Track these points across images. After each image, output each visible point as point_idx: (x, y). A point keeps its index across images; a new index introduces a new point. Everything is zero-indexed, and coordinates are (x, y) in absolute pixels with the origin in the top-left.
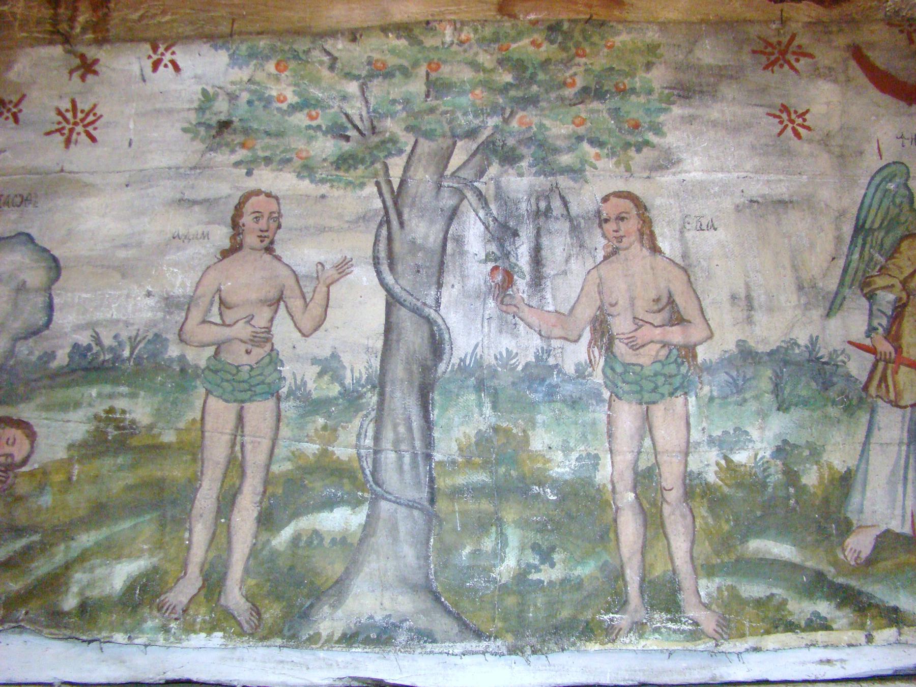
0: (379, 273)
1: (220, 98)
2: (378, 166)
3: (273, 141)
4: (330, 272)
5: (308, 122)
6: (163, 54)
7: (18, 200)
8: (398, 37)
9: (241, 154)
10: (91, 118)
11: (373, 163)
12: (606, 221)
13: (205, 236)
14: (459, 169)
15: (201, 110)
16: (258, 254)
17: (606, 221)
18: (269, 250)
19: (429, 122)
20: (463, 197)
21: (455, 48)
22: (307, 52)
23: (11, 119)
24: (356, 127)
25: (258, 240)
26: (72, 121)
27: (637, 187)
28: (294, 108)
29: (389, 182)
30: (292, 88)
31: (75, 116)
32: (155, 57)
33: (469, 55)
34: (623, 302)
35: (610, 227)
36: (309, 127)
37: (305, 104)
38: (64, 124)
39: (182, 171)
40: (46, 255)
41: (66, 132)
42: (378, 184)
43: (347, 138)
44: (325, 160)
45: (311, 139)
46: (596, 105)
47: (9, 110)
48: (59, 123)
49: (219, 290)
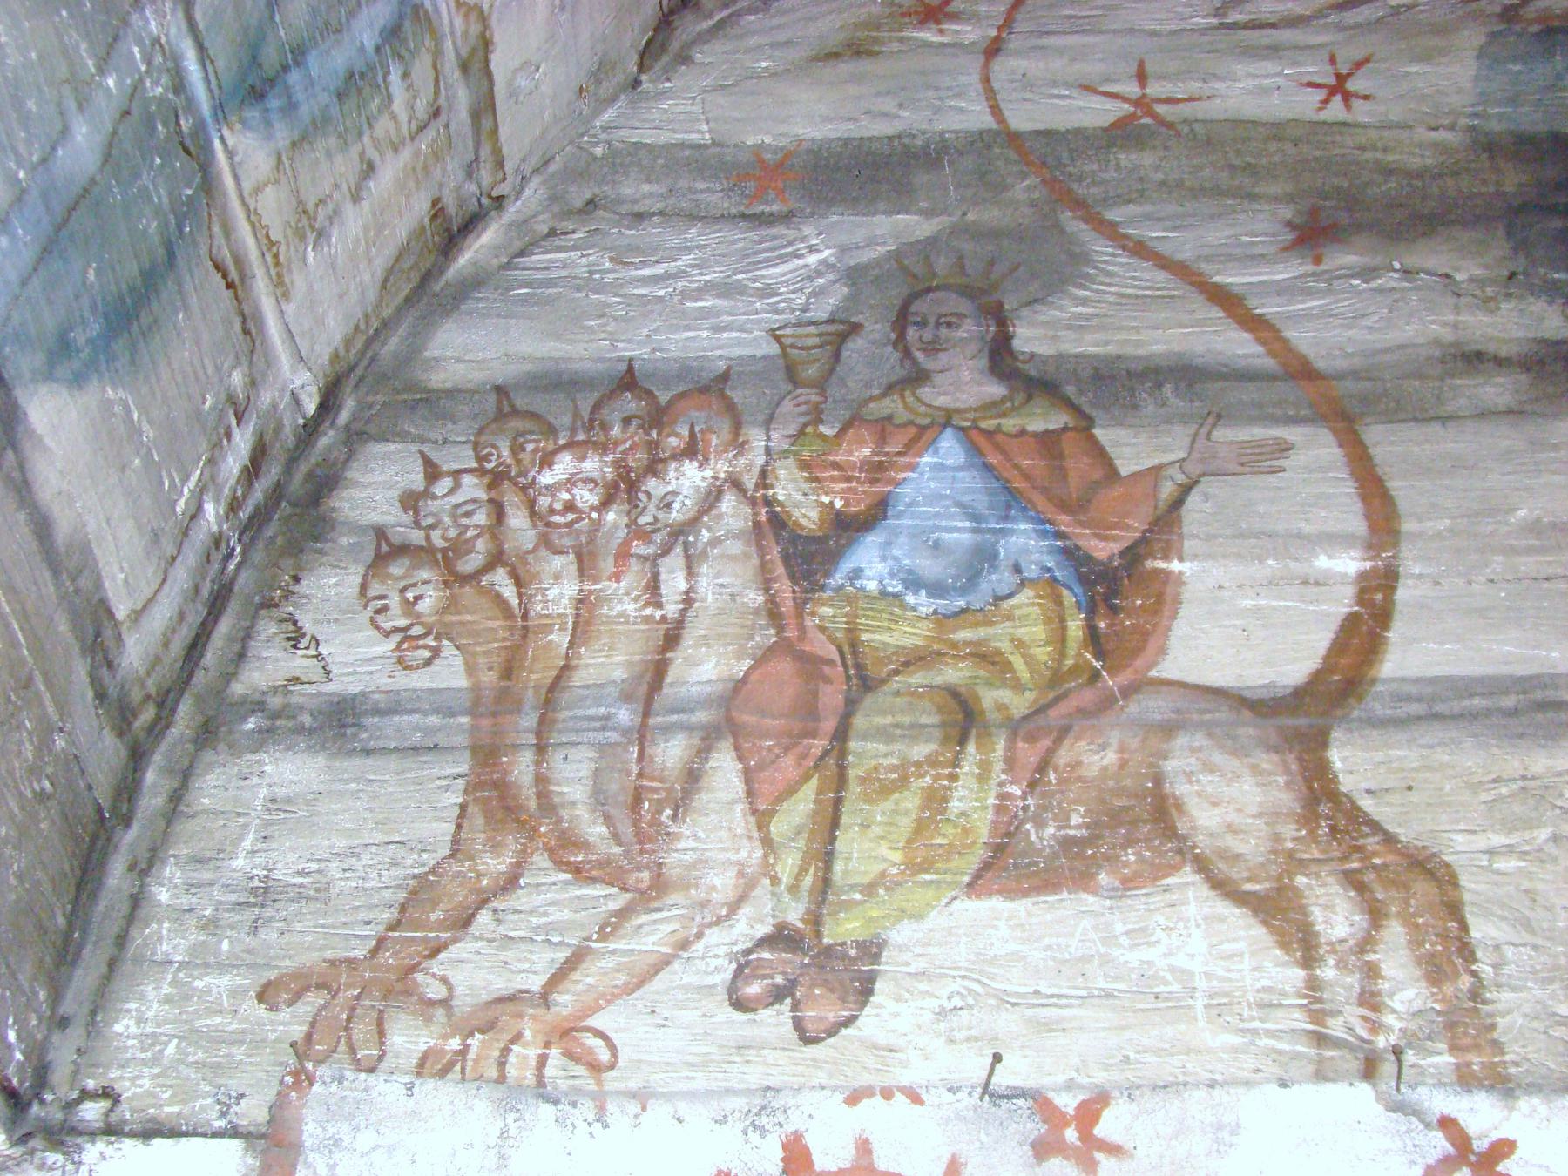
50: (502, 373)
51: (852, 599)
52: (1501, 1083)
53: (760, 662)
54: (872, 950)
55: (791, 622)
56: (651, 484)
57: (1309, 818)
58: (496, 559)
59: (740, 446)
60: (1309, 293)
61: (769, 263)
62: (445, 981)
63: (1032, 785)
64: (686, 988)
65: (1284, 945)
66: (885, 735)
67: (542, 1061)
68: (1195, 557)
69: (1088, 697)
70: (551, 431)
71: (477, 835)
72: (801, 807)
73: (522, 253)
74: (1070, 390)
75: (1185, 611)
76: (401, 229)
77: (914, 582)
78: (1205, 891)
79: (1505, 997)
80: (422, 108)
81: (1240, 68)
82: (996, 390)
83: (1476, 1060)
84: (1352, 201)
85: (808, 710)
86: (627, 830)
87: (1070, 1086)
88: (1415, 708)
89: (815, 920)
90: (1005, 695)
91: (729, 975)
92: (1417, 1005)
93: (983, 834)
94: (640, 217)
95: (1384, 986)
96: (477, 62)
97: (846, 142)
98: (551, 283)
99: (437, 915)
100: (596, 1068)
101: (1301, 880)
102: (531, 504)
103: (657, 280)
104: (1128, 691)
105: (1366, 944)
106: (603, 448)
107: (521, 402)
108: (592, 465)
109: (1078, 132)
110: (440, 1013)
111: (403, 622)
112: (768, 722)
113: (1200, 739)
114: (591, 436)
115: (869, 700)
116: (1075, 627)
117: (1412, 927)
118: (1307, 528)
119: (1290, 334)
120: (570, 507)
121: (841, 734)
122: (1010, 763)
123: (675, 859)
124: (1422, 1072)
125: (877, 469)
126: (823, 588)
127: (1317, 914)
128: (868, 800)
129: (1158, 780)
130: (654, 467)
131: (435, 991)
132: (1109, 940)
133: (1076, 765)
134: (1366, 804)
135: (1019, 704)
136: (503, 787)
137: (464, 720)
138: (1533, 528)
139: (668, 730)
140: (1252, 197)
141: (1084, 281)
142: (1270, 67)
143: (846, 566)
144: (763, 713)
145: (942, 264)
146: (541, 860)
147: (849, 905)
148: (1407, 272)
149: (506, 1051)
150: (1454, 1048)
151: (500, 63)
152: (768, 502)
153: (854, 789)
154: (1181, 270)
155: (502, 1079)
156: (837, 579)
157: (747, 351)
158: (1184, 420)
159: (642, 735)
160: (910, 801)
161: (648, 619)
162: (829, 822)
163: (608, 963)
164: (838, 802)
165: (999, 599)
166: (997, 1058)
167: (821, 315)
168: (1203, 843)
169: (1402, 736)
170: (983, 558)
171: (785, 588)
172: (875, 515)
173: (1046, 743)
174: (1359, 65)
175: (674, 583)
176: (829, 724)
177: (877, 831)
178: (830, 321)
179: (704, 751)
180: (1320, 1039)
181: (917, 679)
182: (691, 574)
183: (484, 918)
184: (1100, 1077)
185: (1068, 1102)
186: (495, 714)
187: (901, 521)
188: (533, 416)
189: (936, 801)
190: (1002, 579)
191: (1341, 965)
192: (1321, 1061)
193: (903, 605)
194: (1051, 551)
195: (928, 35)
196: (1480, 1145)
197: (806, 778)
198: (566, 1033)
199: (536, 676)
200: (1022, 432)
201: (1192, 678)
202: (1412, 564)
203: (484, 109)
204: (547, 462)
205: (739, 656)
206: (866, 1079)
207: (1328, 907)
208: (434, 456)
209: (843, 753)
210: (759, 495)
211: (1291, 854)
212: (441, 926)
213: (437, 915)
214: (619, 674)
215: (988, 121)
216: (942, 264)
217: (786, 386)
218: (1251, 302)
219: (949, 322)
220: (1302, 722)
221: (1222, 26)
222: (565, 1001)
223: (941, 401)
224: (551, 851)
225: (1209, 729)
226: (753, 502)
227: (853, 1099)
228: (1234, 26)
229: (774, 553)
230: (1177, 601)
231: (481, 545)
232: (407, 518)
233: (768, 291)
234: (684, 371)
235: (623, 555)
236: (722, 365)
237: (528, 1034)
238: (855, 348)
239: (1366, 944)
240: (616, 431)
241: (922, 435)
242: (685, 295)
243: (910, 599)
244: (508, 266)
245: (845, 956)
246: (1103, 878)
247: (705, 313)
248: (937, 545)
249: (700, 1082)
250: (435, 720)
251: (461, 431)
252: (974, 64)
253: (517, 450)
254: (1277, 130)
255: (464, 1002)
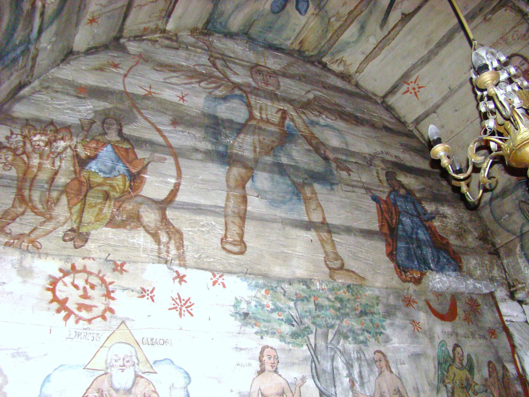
0: (315, 382)
1: (243, 302)
2: (306, 338)
3: (267, 324)
4: (300, 382)
5: (278, 317)
6: (218, 279)
7: (162, 342)
8: (303, 285)
9: (256, 329)
10: (188, 304)
11: (304, 336)
12: (376, 361)
13: (250, 365)
14: (331, 340)
15: (235, 306)
16: (272, 373)
17: (376, 361)
18: (276, 371)
19: (318, 321)
20: (336, 352)
21: (321, 291)
22: (276, 287)
23: (150, 299)
24: (295, 321)
25: (271, 367)
26: (180, 304)
27: (382, 349)
28: (273, 311)
29: (311, 344)
30: (271, 302)
31: (181, 302)
32: (214, 279)
33: (326, 295)
34: (386, 391)
35: (378, 363)
36: (279, 319)
37: (277, 309)
38: (176, 305)
39: (234, 334)
40: (182, 370)
41: (178, 309)
42: (307, 345)
43: (293, 325)
44: (287, 334)
45: (280, 325)
46: (365, 318)
47: (148, 295)
48: (174, 304)
49: (260, 389)
50: (27, 116)
51: (90, 172)
52: (185, 266)
53: (72, 180)
54: (88, 234)
55: (78, 174)
56: (55, 144)
57: (162, 221)
58: (24, 153)
59: (72, 140)
60: (174, 133)
61: (80, 106)
62: (10, 230)
63: (118, 210)
64: (55, 237)
65: (155, 242)
66: (93, 197)
67: (28, 246)
68: (149, 175)
69: (128, 196)
70: (36, 130)
71: (17, 204)
72: (77, 208)
73: (33, 93)
74: (131, 141)
75: (146, 184)
76: (13, 86)
77: (101, 171)
78: (144, 231)
79: (188, 253)
80: (23, 64)
81: (167, 90)
82: (118, 139)
83: (182, 263)
84: (181, 118)
85: (79, 191)
86: (46, 207)
87: (119, 260)
88: (180, 206)
89: (78, 228)
90: (114, 193)
91: (63, 235)
92: (174, 253)
93: (109, 217)
94: (57, 92)
95: (170, 250)
96: (34, 59)
97: (97, 86)
98: (38, 101)
99: (9, 218)
100: (38, 248)
101: (159, 232)
102: (31, 143)
103: (60, 105)
104: (135, 196)
105: (168, 243)
106: (46, 135)
107: (31, 123)
108: (43, 138)
109: (138, 95)
110: (9, 236)
111: (5, 161)
112: (73, 192)
113: (146, 206)
114: (43, 133)
115: (91, 191)
116: (128, 184)
117: (175, 240)
118: (167, 173)
119: (169, 139)
120: (39, 145)
121: (85, 196)
122: (114, 205)
123: (54, 213)
124: (174, 264)
125: (96, 149)
126: (84, 169)
127: (161, 237)
128: (89, 208)
129: (139, 212)
130: (55, 141)
131: (8, 231)
132: (128, 237)
133: (125, 207)
134: (171, 221)
135: (117, 195)
136: (23, 196)
137: (16, 182)
138: (202, 180)
139: (55, 190)
140: (166, 114)
141: (136, 122)
142: (171, 91)
143: (90, 165)
144: (71, 189)
145: (112, 114)
146: (29, 210)
147: (84, 226)
148: (189, 133)
149: (21, 243)
150: (179, 260)
151: (38, 59)
152: (76, 151)
153: (87, 206)
154: (153, 124)
155: (20, 248)
156: (87, 168)
157: (75, 122)
158: (150, 151)
159: (49, 190)
160: (96, 210)
161: (52, 169)
162: (82, 211)
163: (41, 230)
164: (84, 208)
165: (115, 176)
166: (109, 255)
167: (89, 118)
168: (145, 224)
169: (178, 210)
170: (113, 169)
171: (78, 168)
172: (94, 158)
173: (121, 203)
174: (186, 95)
175: (57, 163)
176: (83, 194)
177: (90, 214)
178: (91, 120)
179: (61, 195)
180: (159, 257)
181: (99, 188)
182: (61, 162)
183: (18, 219)
184: (125, 259)
185: (119, 263)
186: (22, 182)
187: (99, 159)
188: (33, 126)
189: (101, 210)
190: (115, 173)
191: (164, 246)
192: (159, 260)
193: (98, 175)
194: (125, 169)
195: (114, 70)
196: (181, 275)
197: (78, 203)
198: (32, 242)
199: (30, 176)
200: (122, 147)
201: (146, 196)
202: (183, 183)
203: (33, 67)
204: (35, 135)
205: (69, 178)
206: (86, 256)
207: (163, 236)
208: (13, 130)
209: (85, 199)
210: (74, 149)
211: (158, 227)
212: (9, 220)
213: (9, 218)
214: (46, 178)
215: (123, 89)
216: (112, 114)
217: (81, 130)
218: (163, 132)
219: (112, 124)
220: (163, 206)
221: (165, 82)
222: (33, 236)
223: (109, 139)
224: (31, 209)
225: (148, 205)
226: (73, 151)
227: (84, 259)
228: (167, 82)
229: (76, 161)
230: (145, 182)
231: (21, 149)
232: (7, 141)
233: (79, 111)
234: (62, 124)
235: (48, 156)
236: (70, 124)
237: (26, 241)
238: (94, 126)
239: (168, 243)
240: (49, 132)
241: (105, 144)
242: (64, 109)
243: (100, 174)
244: (30, 95)
245: (83, 234)
246: (128, 227)
247: (68, 113)
248: (105, 165)
249: (56, 253)
250: (10, 181)
251: (19, 126)
252: (122, 77)
253: (29, 132)
254: (171, 103)
255: (14, 234)
